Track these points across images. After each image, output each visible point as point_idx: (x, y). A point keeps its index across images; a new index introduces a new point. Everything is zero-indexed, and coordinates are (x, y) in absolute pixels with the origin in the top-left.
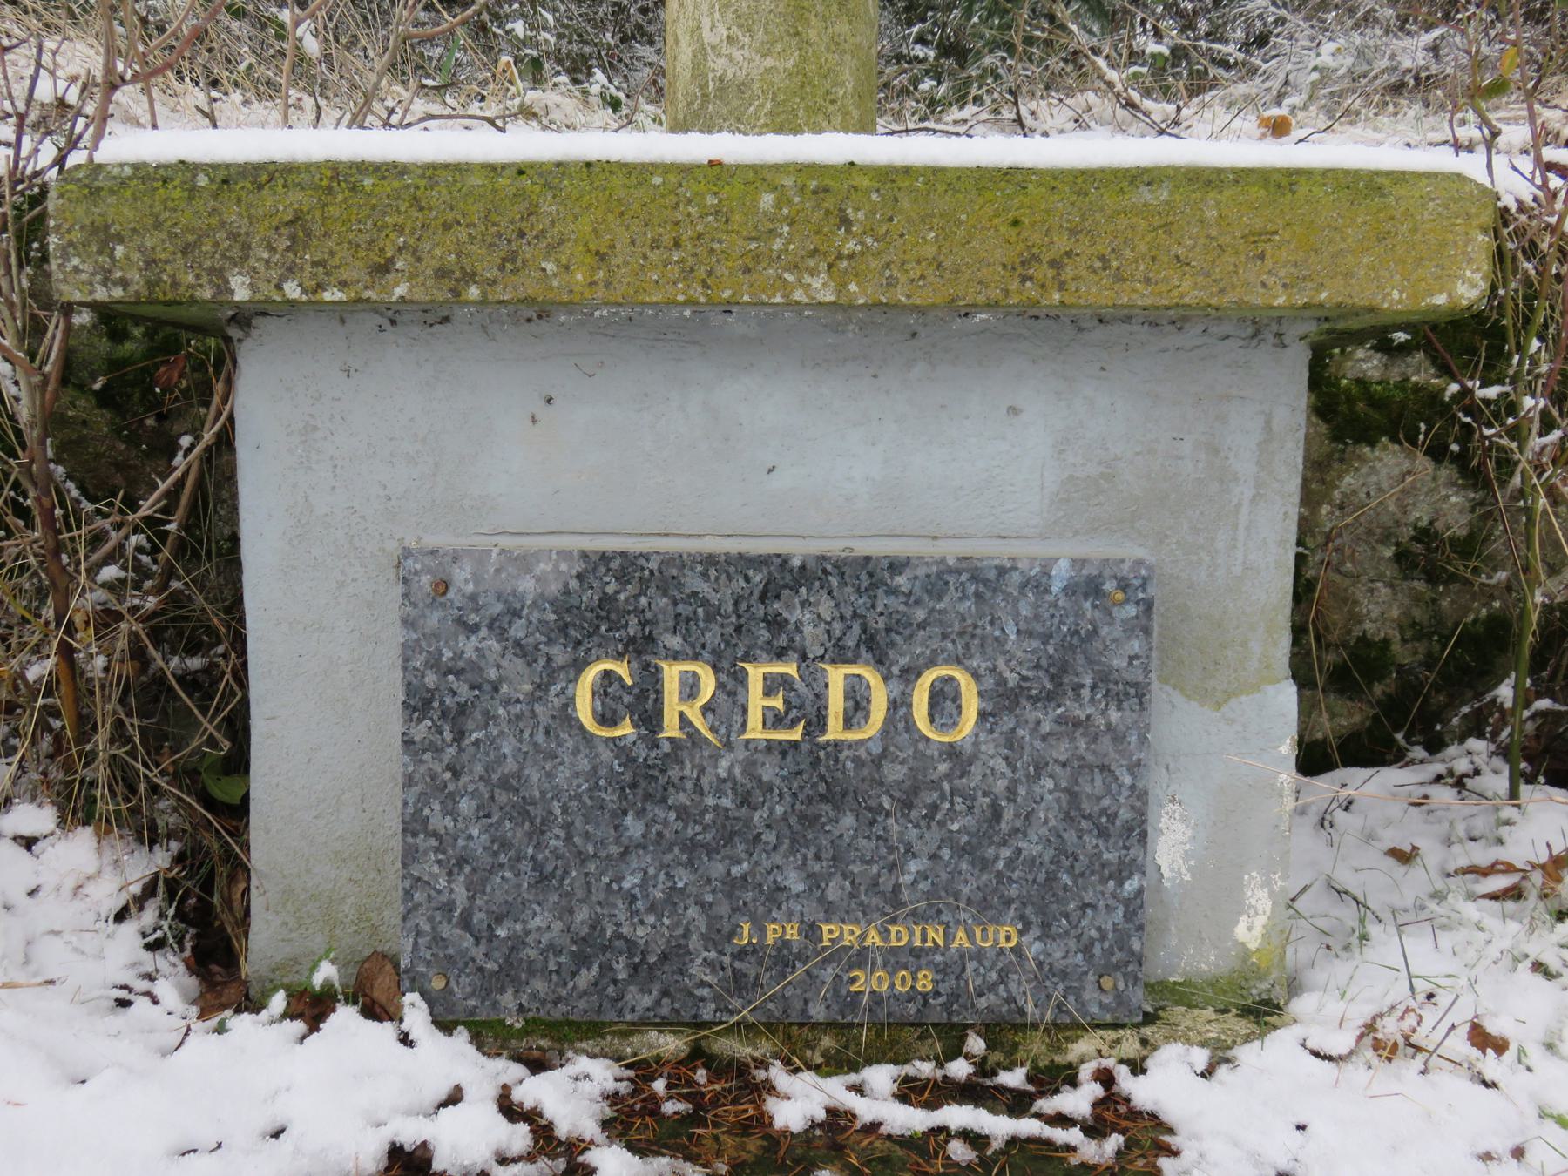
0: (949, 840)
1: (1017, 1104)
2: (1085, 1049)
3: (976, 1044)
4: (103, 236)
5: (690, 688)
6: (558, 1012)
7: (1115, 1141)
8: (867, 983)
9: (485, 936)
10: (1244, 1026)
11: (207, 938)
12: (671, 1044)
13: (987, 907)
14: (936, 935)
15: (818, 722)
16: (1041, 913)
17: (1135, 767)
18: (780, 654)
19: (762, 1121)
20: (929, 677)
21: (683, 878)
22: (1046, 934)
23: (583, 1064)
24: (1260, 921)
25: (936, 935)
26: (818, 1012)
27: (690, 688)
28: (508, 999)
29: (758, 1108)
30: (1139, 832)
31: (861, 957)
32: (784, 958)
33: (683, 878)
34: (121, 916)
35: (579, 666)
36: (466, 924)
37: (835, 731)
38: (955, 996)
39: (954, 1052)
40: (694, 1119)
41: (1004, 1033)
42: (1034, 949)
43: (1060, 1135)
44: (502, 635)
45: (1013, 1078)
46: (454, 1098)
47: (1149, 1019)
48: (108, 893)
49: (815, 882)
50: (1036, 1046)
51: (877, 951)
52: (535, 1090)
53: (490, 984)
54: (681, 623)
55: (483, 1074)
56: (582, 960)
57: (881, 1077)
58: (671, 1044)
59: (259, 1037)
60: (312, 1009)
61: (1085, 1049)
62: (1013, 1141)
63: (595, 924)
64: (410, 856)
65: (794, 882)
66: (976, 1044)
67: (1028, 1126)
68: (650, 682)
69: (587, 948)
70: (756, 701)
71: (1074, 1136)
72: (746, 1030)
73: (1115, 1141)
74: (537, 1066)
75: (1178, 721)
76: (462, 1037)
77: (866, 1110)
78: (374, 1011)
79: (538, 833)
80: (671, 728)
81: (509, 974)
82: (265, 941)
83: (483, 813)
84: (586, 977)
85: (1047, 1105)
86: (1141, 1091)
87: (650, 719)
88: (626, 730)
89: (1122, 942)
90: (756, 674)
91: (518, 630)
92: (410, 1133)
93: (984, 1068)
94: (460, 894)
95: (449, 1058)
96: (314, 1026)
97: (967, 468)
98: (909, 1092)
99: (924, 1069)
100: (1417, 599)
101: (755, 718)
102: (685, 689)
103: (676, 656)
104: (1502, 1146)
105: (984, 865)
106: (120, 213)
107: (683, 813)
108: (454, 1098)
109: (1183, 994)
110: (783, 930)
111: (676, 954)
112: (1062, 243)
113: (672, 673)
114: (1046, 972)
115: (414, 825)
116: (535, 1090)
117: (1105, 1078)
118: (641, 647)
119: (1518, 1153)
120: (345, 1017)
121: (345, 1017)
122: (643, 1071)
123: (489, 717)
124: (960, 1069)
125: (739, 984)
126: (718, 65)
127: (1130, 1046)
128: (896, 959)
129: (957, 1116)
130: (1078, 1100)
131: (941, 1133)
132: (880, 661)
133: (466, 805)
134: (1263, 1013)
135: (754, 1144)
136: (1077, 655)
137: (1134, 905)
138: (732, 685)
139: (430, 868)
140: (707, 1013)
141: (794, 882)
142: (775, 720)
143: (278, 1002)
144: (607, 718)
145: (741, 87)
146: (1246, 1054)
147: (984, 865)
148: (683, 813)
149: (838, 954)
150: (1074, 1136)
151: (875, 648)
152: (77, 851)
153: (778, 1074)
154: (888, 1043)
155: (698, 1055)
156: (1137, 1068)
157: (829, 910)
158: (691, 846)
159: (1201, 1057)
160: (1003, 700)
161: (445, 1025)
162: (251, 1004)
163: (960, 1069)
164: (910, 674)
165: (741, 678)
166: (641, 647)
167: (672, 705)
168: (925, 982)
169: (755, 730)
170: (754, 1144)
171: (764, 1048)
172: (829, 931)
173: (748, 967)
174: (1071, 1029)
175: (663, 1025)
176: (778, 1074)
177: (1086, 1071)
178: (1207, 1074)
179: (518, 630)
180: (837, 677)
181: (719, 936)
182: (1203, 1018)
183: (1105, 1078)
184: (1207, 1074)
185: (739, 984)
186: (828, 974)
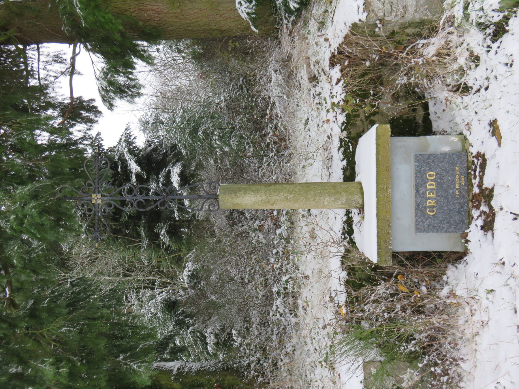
0: (446, 174)
1: (476, 167)
2: (471, 159)
3: (470, 171)
4: (386, 261)
5: (430, 203)
6: (467, 216)
7: (479, 158)
8: (463, 183)
9: (458, 224)
10: (467, 141)
11: (459, 257)
12: (470, 204)
13: (454, 170)
14: (457, 176)
15: (433, 189)
16: (454, 164)
17: (437, 155)
18: (426, 193)
19: (478, 194)
20: (428, 177)
21: (451, 203)
22: (457, 164)
23: (473, 213)
24: (455, 138)
25: (457, 176)
26: (466, 188)
27: (430, 203)
28: (466, 221)
29: (53, 106)
30: (445, 154)
31: (460, 184)
32: (460, 192)
33: (451, 203)
34: (456, 267)
35: (428, 214)
36: (457, 226)
37: (434, 187)
38: (464, 173)
39: (470, 173)
40: (478, 201)
41: (468, 168)
42: (458, 165)
43: (479, 163)
44: (424, 222)
45: (473, 167)
46: (476, 225)
47: (467, 152)
48: (454, 269)
49: (451, 189)
50: (470, 164)
51: (459, 182)
52: (475, 217)
53: (464, 223)
54: (423, 204)
55: (474, 222)
56: (461, 213)
57: (473, 181)
58: (470, 204)
59: (470, 246)
60: (467, 241)
61: (471, 159)
62: (480, 168)
63: (457, 212)
64: (449, 232)
65: (451, 191)
66: (470, 171)
67: (478, 167)
68: (429, 207)
69: (459, 213)
70: (431, 195)
71: (479, 162)
72: (469, 195)
73: (479, 158)
74: (473, 218)
75: (431, 150)
76: (470, 226)
77: (477, 183)
78: (467, 236)
79: (447, 218)
80: (435, 205)
81: (462, 221)
82: (459, 249)
83: (444, 224)
84: (463, 213)
85: (476, 164)
86: (475, 154)
87: (434, 207)
88: (435, 209)
89: (457, 155)
90: (428, 196)
91: (424, 221)
92: (479, 228)
93: (472, 170)
94: (454, 226)
95: (472, 227)
96: (469, 241)
97: (404, 173)
98: (475, 178)
99: (472, 177)
100: (402, 99)
101: (433, 196)
102: (431, 203)
103: (426, 204)
104: (478, 122)
105: (449, 171)
106: (383, 259)
107: (444, 203)
108: (476, 225)
109: (464, 146)
110: (457, 192)
111: (460, 203)
112: (385, 167)
113: (428, 204)
114: (461, 163)
115: (446, 231)
116: (475, 217)
117: (473, 157)
118: (426, 208)
119: (479, 120)
120: (468, 238)
121: (468, 238)
122: (473, 207)
123: (434, 224)
124: (473, 173)
125: (463, 197)
126: (344, 202)
127: (470, 154)
128: (460, 180)
129: (477, 174)
130: (476, 161)
131: (479, 175)
132: (427, 183)
133: (444, 226)
134: (465, 138)
135: (481, 195)
136: (424, 162)
137: (453, 154)
138: (429, 198)
139: (450, 230)
140: (467, 200)
141: (451, 191)
142: (433, 194)
143: (466, 245)
144: (433, 211)
145: (347, 199)
146: (470, 142)
147: (449, 171)
148: (444, 203)
149: (460, 186)
150: (479, 162)
151: (425, 183)
152: (449, 272)
153: (474, 192)
154: (471, 180)
155: (472, 201)
156: (472, 154)
157: (455, 187)
158: (448, 202)
159: (470, 147)
160: (431, 170)
161: (469, 228)
162: (466, 249)
163: (473, 173)
164: (428, 179)
165: (429, 197)
166: (426, 208)
167: (432, 204)
168: (463, 177)
169: (435, 196)
170: (481, 195)
171: (471, 194)
172: (457, 187)
173: (462, 196)
174: (468, 161)
175: (468, 205)
176: (474, 192)
177: (473, 159)
178: (473, 146)
179: (424, 221)
180: (428, 187)
181: (458, 199)
182: (467, 145)
183: (473, 157)
184: (473, 146)
185: (463, 197)
186: (462, 187)
